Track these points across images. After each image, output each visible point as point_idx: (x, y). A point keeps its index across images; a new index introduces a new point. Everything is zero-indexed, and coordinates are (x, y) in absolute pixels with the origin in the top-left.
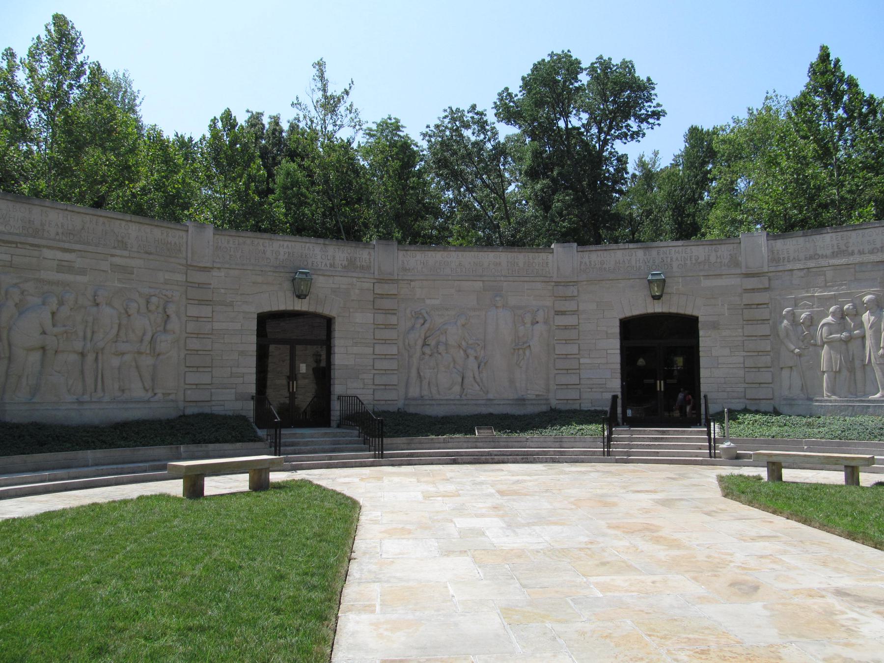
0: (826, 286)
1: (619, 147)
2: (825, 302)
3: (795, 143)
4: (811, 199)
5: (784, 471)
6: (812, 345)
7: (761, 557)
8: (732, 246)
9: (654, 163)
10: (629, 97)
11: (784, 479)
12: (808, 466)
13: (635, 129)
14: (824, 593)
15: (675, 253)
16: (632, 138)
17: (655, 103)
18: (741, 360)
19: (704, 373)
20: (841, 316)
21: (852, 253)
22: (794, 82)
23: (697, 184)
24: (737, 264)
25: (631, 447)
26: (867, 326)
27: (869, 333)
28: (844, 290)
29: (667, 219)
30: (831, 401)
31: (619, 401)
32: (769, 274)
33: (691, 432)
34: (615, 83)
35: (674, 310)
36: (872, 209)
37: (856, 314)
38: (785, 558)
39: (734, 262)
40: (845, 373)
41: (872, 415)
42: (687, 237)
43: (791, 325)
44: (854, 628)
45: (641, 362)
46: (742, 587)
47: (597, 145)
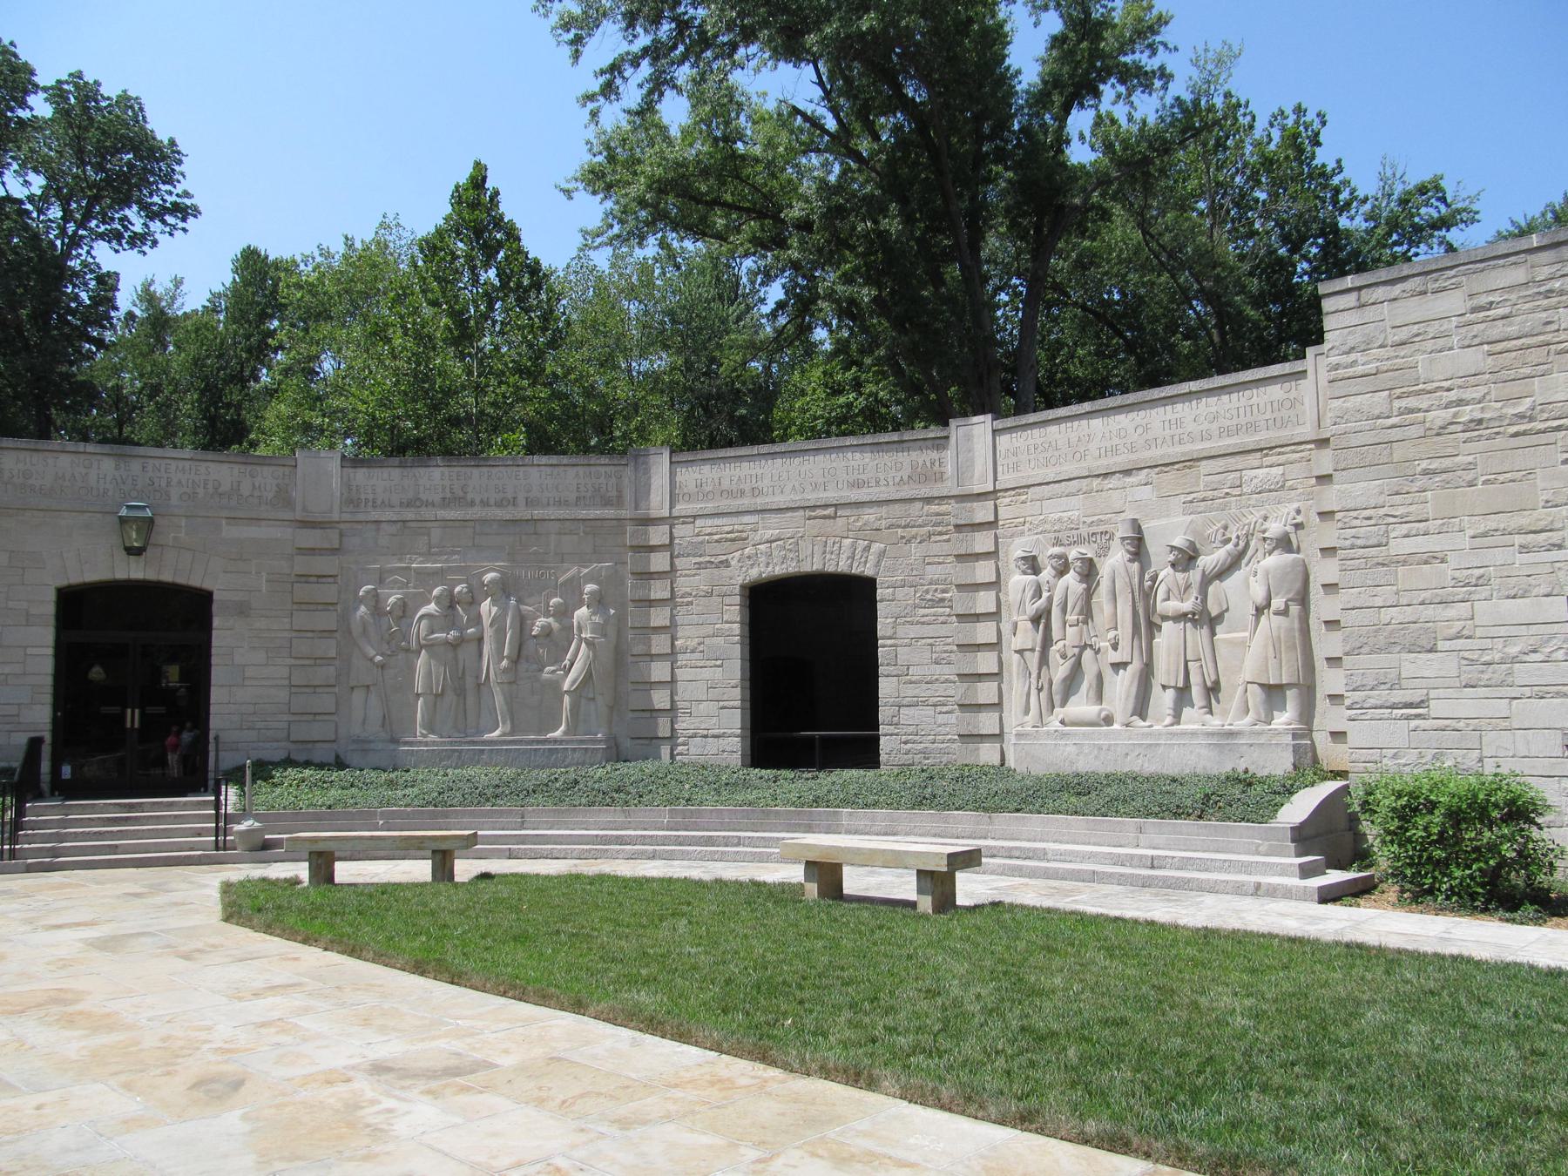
0: (429, 553)
1: (105, 256)
2: (427, 578)
3: (416, 311)
4: (435, 408)
5: (338, 865)
6: (400, 648)
7: (263, 1025)
8: (281, 469)
9: (173, 298)
10: (130, 164)
11: (337, 880)
12: (382, 853)
13: (138, 228)
14: (351, 1073)
15: (181, 473)
16: (132, 244)
17: (179, 189)
18: (285, 672)
19: (216, 695)
20: (450, 602)
21: (472, 504)
22: (426, 212)
23: (249, 350)
24: (289, 504)
25: (62, 838)
26: (486, 621)
27: (488, 634)
28: (455, 561)
29: (187, 408)
30: (426, 744)
31: (46, 750)
32: (342, 526)
33: (185, 803)
34: (104, 132)
35: (167, 577)
36: (520, 437)
37: (473, 602)
38: (304, 1022)
39: (284, 498)
40: (450, 697)
41: (486, 764)
42: (225, 444)
43: (372, 614)
44: (385, 1127)
45: (97, 673)
46: (215, 1086)
47: (58, 243)
